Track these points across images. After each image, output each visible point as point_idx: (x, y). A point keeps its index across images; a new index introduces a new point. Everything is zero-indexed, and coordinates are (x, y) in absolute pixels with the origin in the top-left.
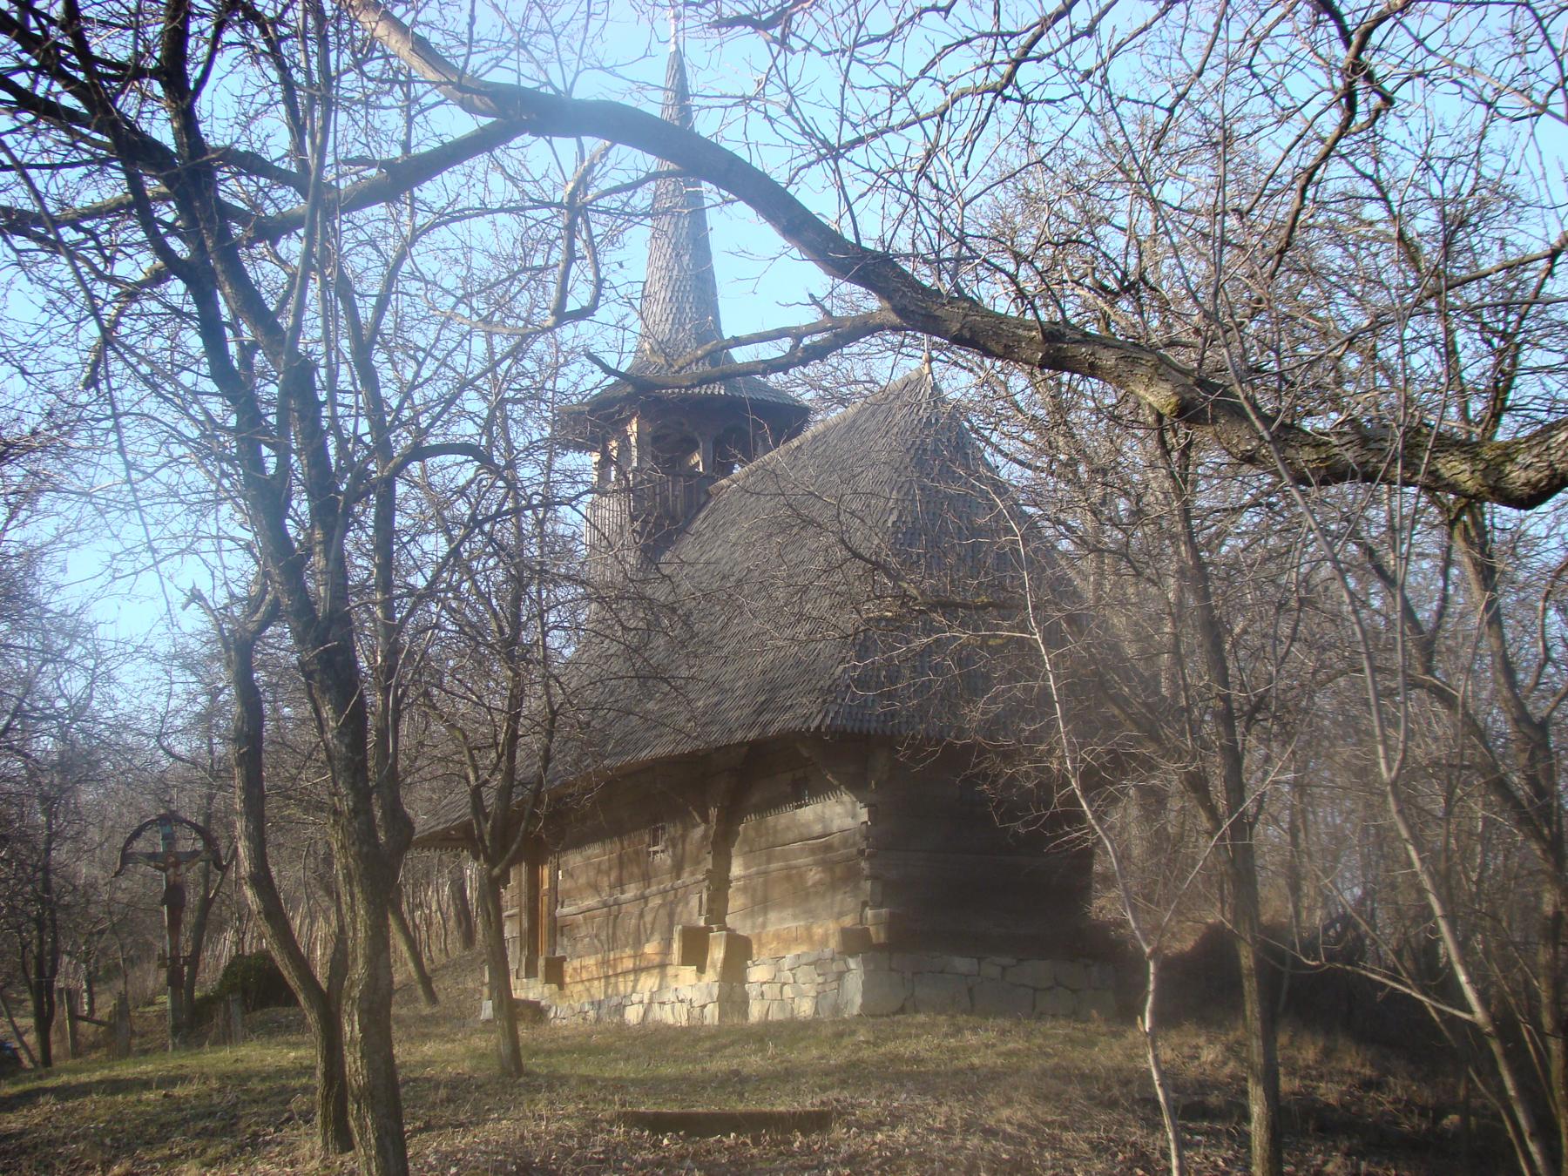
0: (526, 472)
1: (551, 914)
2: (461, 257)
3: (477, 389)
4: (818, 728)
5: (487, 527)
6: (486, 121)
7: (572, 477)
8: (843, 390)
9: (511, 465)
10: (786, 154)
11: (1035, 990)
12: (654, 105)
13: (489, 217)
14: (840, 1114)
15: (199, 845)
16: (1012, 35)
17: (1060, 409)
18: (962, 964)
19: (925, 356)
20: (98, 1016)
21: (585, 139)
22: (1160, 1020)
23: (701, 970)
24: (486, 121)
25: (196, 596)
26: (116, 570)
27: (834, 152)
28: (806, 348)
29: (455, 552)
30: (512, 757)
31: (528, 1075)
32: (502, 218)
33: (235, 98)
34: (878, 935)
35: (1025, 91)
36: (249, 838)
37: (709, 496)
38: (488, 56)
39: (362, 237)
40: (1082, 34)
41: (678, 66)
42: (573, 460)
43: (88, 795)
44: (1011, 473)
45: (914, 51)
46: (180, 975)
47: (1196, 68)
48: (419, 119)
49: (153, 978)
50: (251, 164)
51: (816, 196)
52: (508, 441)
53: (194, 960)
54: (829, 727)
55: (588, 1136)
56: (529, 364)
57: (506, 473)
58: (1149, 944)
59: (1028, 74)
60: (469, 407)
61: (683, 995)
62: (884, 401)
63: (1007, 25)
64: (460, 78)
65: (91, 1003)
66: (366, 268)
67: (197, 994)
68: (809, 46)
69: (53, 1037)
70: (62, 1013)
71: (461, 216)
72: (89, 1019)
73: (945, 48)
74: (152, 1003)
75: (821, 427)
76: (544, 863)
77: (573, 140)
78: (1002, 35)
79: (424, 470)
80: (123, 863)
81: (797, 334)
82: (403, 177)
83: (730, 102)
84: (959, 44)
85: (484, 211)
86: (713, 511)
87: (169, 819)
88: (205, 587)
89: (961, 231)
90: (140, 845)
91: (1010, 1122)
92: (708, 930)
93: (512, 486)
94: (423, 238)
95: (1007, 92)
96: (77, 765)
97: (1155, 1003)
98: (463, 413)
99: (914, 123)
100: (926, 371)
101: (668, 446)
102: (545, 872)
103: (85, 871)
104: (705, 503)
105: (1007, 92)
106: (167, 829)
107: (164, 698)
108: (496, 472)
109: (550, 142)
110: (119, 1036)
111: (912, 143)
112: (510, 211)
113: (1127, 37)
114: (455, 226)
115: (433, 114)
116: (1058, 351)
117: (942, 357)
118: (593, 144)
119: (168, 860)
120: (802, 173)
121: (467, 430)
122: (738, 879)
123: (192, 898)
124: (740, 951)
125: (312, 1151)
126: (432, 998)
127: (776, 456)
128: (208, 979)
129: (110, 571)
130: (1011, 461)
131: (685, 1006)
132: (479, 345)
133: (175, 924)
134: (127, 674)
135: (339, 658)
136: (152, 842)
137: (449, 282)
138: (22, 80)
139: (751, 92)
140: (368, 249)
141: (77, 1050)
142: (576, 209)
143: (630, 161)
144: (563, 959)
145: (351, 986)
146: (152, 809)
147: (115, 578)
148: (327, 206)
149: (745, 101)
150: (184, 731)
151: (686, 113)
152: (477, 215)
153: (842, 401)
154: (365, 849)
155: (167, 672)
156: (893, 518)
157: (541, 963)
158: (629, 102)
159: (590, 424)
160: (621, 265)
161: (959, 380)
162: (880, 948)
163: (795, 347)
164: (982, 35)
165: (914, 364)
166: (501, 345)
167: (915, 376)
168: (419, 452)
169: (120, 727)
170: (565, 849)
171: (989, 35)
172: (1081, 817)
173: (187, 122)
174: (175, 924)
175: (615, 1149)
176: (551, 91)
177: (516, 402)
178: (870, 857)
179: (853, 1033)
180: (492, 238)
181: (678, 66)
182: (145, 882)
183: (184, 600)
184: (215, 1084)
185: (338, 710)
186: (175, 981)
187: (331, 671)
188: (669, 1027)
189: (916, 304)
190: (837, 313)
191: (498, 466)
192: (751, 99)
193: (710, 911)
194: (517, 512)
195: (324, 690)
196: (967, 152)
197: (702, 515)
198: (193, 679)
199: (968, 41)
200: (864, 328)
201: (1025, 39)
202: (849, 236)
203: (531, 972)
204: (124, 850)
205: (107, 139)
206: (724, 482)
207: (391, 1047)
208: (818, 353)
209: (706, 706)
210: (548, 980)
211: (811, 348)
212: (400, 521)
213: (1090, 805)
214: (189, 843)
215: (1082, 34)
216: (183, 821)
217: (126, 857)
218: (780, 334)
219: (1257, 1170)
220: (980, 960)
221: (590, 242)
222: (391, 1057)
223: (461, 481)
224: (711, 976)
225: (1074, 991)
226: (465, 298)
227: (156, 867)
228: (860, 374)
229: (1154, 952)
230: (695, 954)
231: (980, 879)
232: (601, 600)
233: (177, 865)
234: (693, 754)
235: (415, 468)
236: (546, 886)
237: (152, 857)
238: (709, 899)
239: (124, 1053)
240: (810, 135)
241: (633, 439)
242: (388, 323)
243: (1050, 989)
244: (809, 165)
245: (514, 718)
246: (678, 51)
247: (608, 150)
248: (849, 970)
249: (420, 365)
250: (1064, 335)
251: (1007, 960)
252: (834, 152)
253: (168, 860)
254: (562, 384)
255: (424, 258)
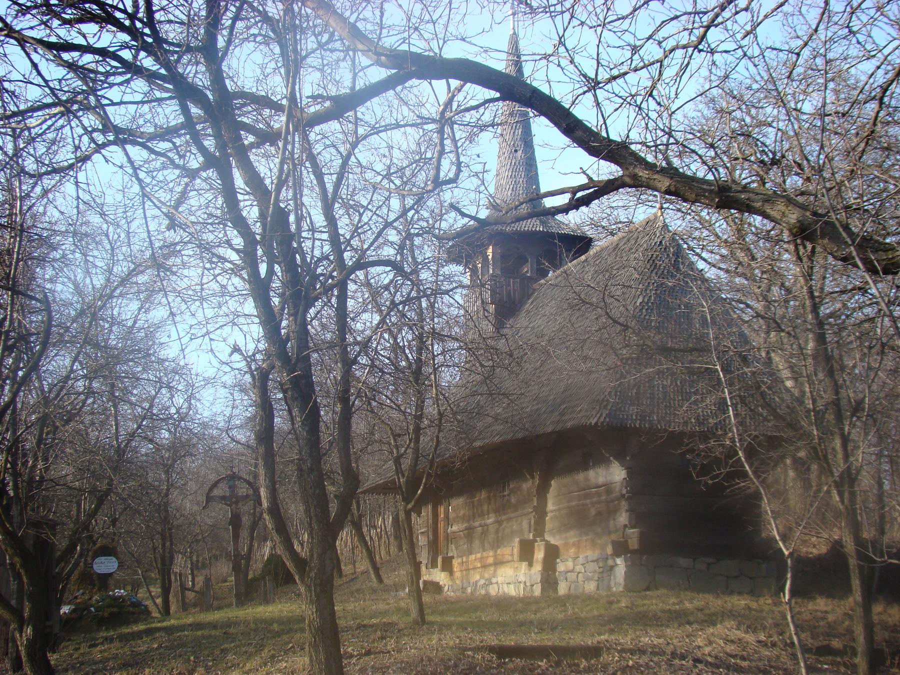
0: (425, 275)
1: (445, 531)
2: (387, 154)
3: (395, 228)
4: (596, 423)
5: (401, 307)
6: (394, 71)
7: (448, 278)
8: (613, 227)
9: (416, 272)
10: (570, 87)
11: (728, 577)
12: (499, 63)
13: (402, 129)
14: (608, 649)
15: (251, 492)
16: (705, 13)
17: (740, 233)
18: (684, 562)
19: (658, 205)
20: (196, 589)
21: (451, 81)
22: (793, 593)
23: (531, 565)
24: (394, 71)
25: (236, 349)
26: (193, 334)
27: (593, 85)
28: (578, 199)
29: (382, 321)
30: (417, 440)
31: (428, 624)
32: (408, 129)
33: (250, 65)
34: (634, 544)
35: (713, 46)
36: (267, 487)
37: (534, 290)
38: (399, 37)
39: (328, 143)
40: (742, 10)
41: (514, 41)
42: (454, 269)
43: (191, 464)
44: (712, 274)
45: (644, 24)
46: (240, 564)
47: (814, 27)
48: (361, 74)
49: (224, 568)
50: (263, 102)
51: (585, 112)
52: (414, 258)
53: (248, 557)
54: (602, 423)
55: (460, 659)
56: (426, 214)
57: (412, 276)
58: (787, 549)
59: (714, 35)
60: (391, 238)
61: (511, 578)
62: (633, 234)
63: (700, 6)
64: (376, 48)
65: (193, 581)
66: (330, 159)
67: (250, 577)
68: (582, 24)
69: (171, 598)
70: (175, 586)
71: (387, 128)
72: (192, 590)
73: (663, 22)
74: (226, 581)
75: (598, 248)
76: (441, 504)
77: (444, 81)
78: (698, 13)
79: (366, 276)
80: (207, 501)
81: (574, 191)
82: (342, 106)
83: (538, 57)
84: (672, 19)
85: (398, 126)
86: (536, 298)
87: (233, 477)
88: (241, 344)
89: (670, 129)
90: (216, 492)
91: (709, 655)
92: (534, 541)
93: (417, 284)
94: (364, 142)
95: (700, 47)
96: (181, 448)
97: (792, 585)
98: (387, 242)
99: (642, 68)
100: (659, 214)
101: (510, 263)
102: (441, 510)
103: (188, 506)
104: (532, 294)
105: (700, 47)
106: (231, 483)
107: (230, 409)
108: (406, 276)
109: (430, 83)
110: (206, 599)
111: (643, 79)
112: (412, 125)
113: (770, 11)
114: (382, 135)
115: (367, 71)
116: (725, 197)
117: (671, 207)
118: (455, 83)
119: (232, 500)
120: (580, 98)
121: (389, 252)
122: (552, 511)
123: (246, 520)
124: (553, 554)
125: (304, 665)
126: (380, 580)
127: (571, 266)
128: (256, 567)
129: (189, 335)
130: (708, 265)
131: (522, 586)
132: (395, 203)
133: (236, 536)
134: (207, 395)
135: (303, 381)
136: (222, 490)
137: (379, 167)
138: (126, 55)
139: (550, 52)
140: (332, 150)
141: (185, 606)
142: (445, 121)
143: (477, 93)
144: (453, 557)
145: (310, 570)
146: (224, 473)
147: (191, 339)
148: (303, 124)
149: (546, 57)
150: (241, 427)
151: (520, 70)
152: (393, 128)
153: (612, 234)
154: (317, 491)
155: (232, 394)
156: (640, 300)
157: (440, 559)
158: (479, 60)
159: (465, 246)
160: (478, 156)
161: (677, 218)
162: (633, 552)
163: (571, 199)
164: (685, 14)
165: (654, 211)
166: (409, 202)
167: (652, 218)
168: (362, 264)
169: (204, 425)
170: (452, 497)
171: (690, 13)
172: (743, 475)
173: (218, 78)
174: (236, 536)
175: (475, 667)
176: (432, 54)
177: (418, 235)
178: (629, 499)
179: (618, 601)
180: (405, 141)
181: (514, 41)
182: (220, 513)
183: (230, 350)
184: (252, 625)
185: (302, 411)
186: (237, 569)
187: (302, 390)
188: (512, 597)
189: (631, 168)
190: (595, 179)
191: (406, 273)
192: (550, 56)
193: (535, 530)
194: (418, 298)
195: (294, 399)
196: (677, 84)
197: (530, 301)
198: (246, 398)
199: (676, 17)
200: (609, 187)
201: (711, 15)
202: (604, 134)
203: (434, 565)
204: (208, 494)
205: (171, 87)
206: (542, 281)
207: (333, 606)
208: (586, 201)
209: (531, 411)
210: (443, 570)
211: (580, 200)
212: (350, 303)
213: (750, 468)
214: (243, 490)
215: (742, 10)
216: (240, 478)
217: (209, 499)
218: (562, 192)
219: (27, 669)
220: (694, 559)
221: (454, 141)
222: (333, 613)
223: (386, 282)
224: (538, 568)
225: (751, 578)
226: (388, 176)
227: (226, 504)
228: (623, 218)
229: (791, 554)
230: (526, 553)
231: (696, 521)
232: (469, 350)
233: (237, 503)
234: (524, 438)
235: (360, 274)
236: (442, 516)
237: (223, 498)
238: (535, 523)
239: (209, 608)
240: (585, 76)
241: (490, 257)
242: (343, 192)
243: (736, 577)
244: (584, 93)
245: (419, 417)
246: (514, 33)
247: (462, 87)
248: (617, 565)
249: (361, 215)
250: (731, 188)
251: (710, 560)
252: (593, 85)
253: (232, 500)
254: (444, 225)
255: (362, 154)
